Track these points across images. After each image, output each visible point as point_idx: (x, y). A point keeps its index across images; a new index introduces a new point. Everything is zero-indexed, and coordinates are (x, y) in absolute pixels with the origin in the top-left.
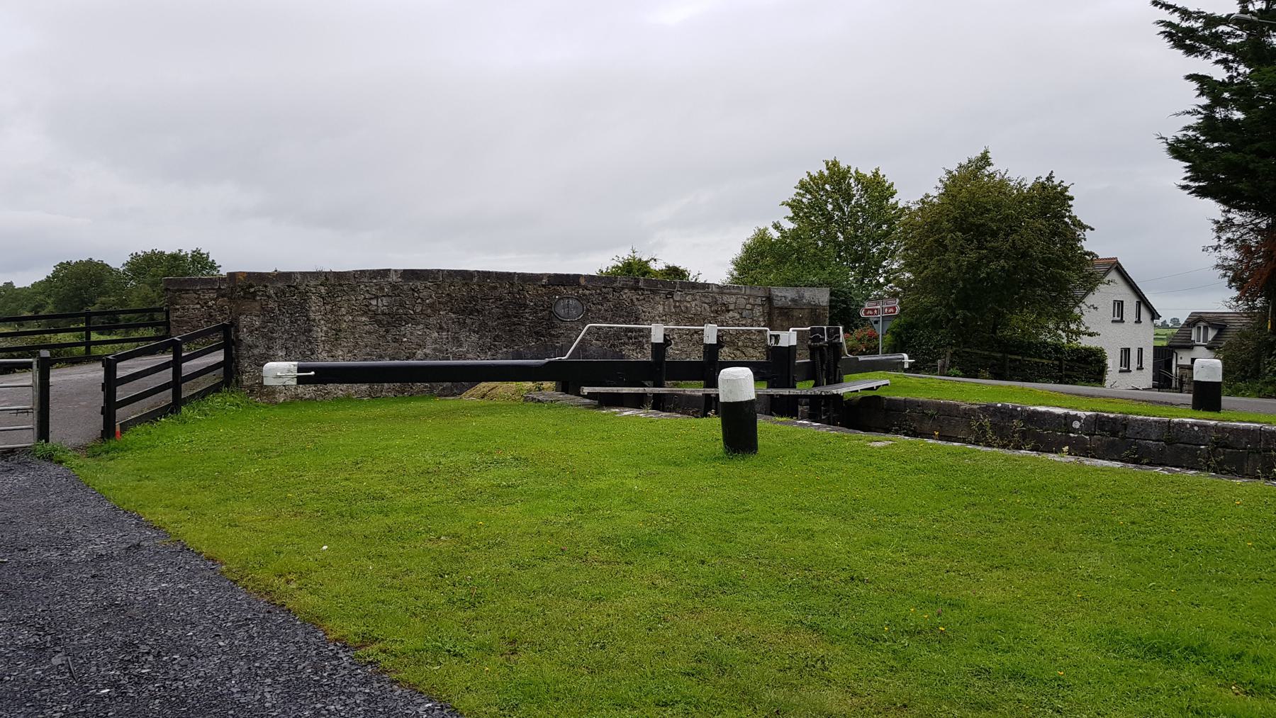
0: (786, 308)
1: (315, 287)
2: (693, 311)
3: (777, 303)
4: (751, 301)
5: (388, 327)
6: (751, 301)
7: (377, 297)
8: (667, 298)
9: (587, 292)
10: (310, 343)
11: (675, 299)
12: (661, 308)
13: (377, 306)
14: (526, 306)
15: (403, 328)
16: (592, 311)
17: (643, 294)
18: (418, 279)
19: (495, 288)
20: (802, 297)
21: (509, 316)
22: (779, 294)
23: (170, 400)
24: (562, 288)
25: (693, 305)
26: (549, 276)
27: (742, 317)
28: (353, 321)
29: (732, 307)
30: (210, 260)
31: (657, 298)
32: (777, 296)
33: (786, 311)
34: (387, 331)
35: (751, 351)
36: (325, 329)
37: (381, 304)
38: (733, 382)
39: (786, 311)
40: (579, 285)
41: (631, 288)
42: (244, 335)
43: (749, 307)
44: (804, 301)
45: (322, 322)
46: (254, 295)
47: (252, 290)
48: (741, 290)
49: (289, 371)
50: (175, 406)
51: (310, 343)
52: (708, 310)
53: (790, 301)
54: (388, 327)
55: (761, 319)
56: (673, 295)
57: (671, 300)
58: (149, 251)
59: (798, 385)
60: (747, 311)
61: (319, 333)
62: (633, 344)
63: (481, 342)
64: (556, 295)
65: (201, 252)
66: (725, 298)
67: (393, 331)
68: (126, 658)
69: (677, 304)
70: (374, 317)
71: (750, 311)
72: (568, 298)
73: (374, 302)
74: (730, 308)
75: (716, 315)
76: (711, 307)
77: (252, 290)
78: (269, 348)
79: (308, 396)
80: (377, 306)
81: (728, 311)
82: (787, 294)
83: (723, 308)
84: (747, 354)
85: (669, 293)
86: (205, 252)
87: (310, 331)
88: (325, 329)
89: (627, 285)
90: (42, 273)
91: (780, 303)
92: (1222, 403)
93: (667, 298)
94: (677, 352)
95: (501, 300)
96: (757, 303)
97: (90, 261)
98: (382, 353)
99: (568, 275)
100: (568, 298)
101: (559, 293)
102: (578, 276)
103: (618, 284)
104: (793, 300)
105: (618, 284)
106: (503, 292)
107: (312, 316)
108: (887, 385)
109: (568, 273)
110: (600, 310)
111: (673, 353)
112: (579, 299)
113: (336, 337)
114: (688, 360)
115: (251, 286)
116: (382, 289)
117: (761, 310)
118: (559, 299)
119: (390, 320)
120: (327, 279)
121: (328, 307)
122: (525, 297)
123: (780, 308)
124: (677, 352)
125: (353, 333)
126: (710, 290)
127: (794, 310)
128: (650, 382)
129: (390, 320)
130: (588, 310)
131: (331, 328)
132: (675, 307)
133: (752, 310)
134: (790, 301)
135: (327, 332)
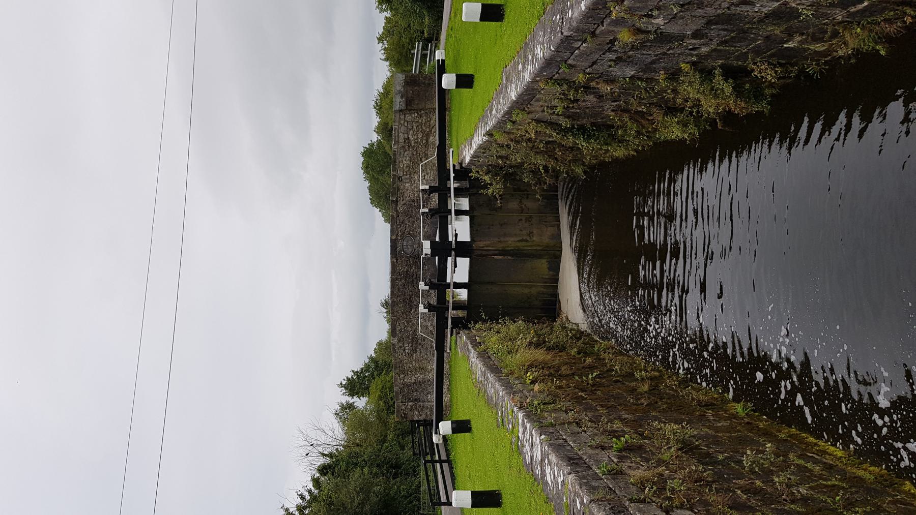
0: (407, 101)
1: (400, 379)
2: (409, 162)
3: (403, 107)
4: (402, 122)
5: (418, 344)
6: (402, 122)
7: (405, 349)
8: (402, 180)
9: (400, 233)
10: (425, 382)
11: (402, 175)
12: (407, 185)
13: (408, 349)
14: (407, 271)
15: (419, 337)
16: (410, 231)
17: (400, 197)
18: (395, 329)
19: (399, 289)
20: (400, 92)
21: (413, 281)
22: (398, 106)
23: (447, 464)
24: (398, 249)
25: (405, 162)
26: (392, 258)
27: (412, 129)
28: (415, 361)
29: (406, 136)
30: (368, 146)
31: (402, 187)
32: (399, 107)
33: (408, 102)
34: (420, 344)
35: (432, 122)
36: (419, 375)
37: (408, 347)
38: (448, 84)
39: (408, 102)
40: (396, 239)
41: (397, 205)
42: (422, 418)
43: (406, 124)
44: (402, 90)
45: (416, 376)
46: (405, 414)
47: (403, 415)
48: (396, 128)
49: (437, 437)
50: (448, 461)
51: (425, 382)
52: (408, 152)
53: (402, 99)
54: (418, 344)
55: (413, 115)
56: (400, 177)
57: (403, 178)
58: (362, 171)
59: (449, 208)
60: (409, 125)
61: (421, 377)
62: (427, 204)
63: (425, 296)
64: (401, 253)
65: (363, 152)
66: (401, 141)
67: (420, 341)
68: (580, 43)
69: (405, 173)
70: (414, 350)
71: (409, 123)
72: (403, 246)
73: (407, 351)
74: (407, 137)
75: (411, 147)
76: (406, 150)
77: (403, 415)
78: (427, 408)
79: (448, 383)
80: (408, 349)
81: (408, 138)
82: (398, 101)
83: (407, 141)
84: (434, 124)
85: (399, 179)
86: (363, 149)
87: (420, 382)
88: (419, 375)
89: (395, 208)
90: (377, 214)
91: (404, 105)
92: (462, 434)
93: (402, 180)
94: (432, 173)
95: (405, 285)
96: (403, 118)
97: (372, 202)
98: (430, 346)
99: (391, 246)
100: (403, 246)
101: (400, 251)
102: (391, 240)
103: (394, 215)
104: (402, 97)
105: (394, 215)
106: (400, 283)
107: (413, 381)
108: (453, 151)
109: (390, 246)
110: (409, 226)
111: (434, 301)
112: (402, 239)
113: (423, 369)
114: (437, 165)
115: (401, 416)
116: (401, 347)
117: (408, 115)
118: (404, 251)
119: (415, 343)
120: (397, 373)
121: (409, 373)
122: (403, 271)
123: (407, 105)
124: (432, 173)
125: (421, 361)
126: (396, 150)
127: (408, 96)
128: (446, 330)
129: (415, 343)
130: (409, 233)
131: (419, 372)
132: (406, 175)
133: (408, 122)
134: (402, 99)
135: (420, 374)
